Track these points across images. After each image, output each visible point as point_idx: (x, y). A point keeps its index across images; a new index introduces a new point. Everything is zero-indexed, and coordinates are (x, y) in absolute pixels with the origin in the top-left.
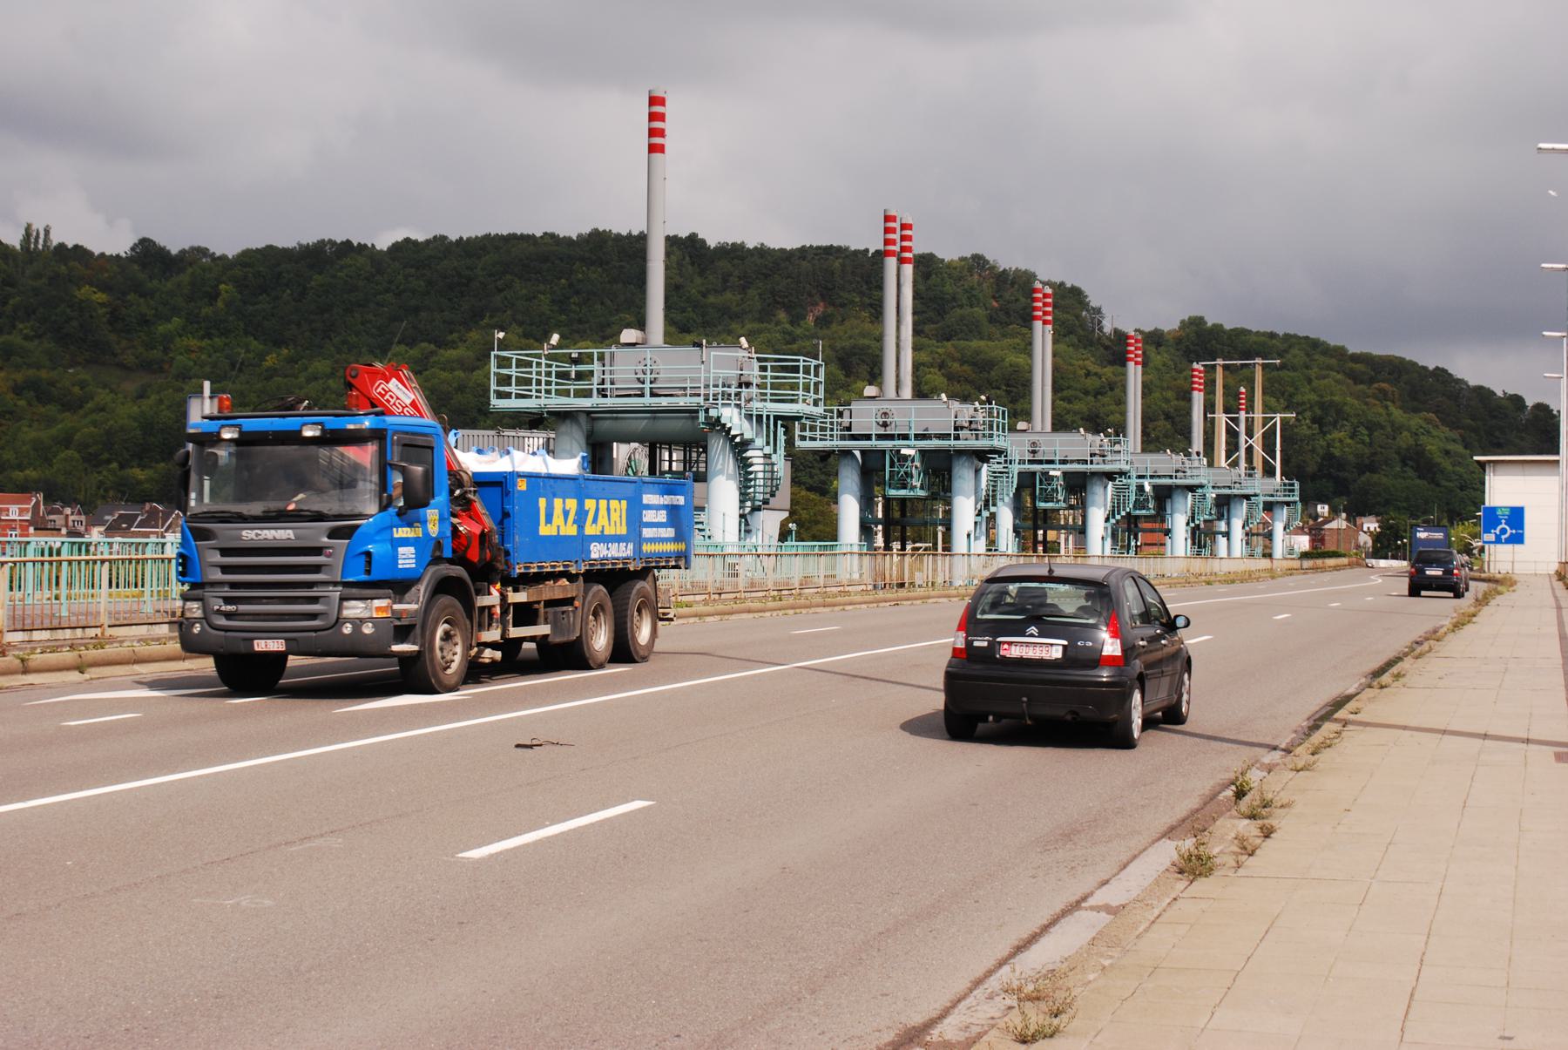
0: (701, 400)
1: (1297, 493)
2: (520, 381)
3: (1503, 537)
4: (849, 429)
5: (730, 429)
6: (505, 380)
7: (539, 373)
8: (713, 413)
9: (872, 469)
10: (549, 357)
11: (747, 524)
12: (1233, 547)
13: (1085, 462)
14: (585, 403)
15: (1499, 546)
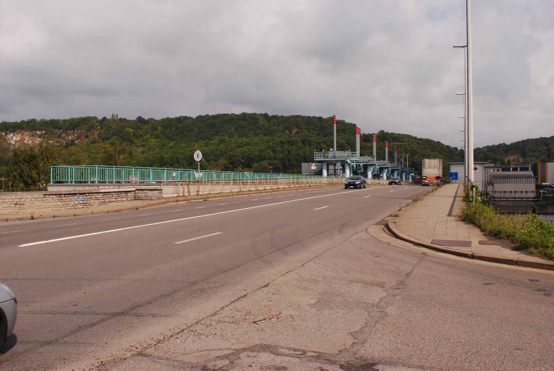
13: (367, 162)
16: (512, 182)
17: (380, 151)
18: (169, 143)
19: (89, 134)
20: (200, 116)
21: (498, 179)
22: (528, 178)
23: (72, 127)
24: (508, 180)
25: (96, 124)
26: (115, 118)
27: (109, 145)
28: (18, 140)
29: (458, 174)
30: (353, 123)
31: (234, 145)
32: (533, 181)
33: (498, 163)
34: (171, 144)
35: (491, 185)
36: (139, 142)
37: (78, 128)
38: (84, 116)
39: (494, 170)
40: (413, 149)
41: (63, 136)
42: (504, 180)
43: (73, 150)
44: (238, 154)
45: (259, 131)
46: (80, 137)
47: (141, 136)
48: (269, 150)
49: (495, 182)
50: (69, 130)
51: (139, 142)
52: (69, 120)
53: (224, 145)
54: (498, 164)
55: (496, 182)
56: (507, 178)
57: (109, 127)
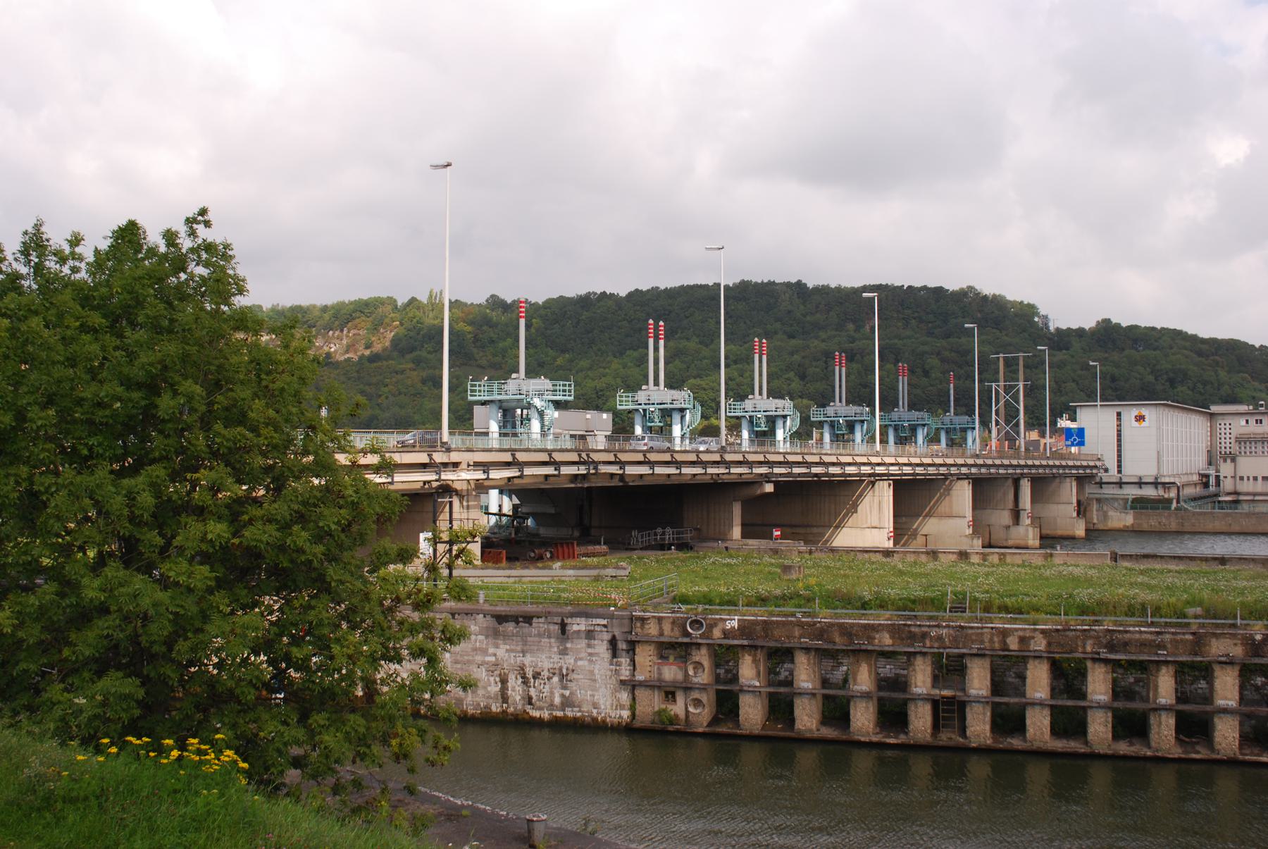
9: (948, 432)
16: (1256, 452)
17: (1084, 372)
18: (555, 359)
19: (373, 339)
20: (941, 287)
21: (1248, 443)
23: (337, 323)
25: (392, 315)
26: (436, 298)
27: (411, 365)
29: (1087, 433)
30: (1026, 303)
31: (706, 361)
33: (1263, 402)
34: (559, 361)
35: (1229, 461)
36: (486, 356)
37: (350, 324)
38: (365, 296)
39: (1247, 422)
40: (1178, 366)
41: (317, 344)
43: (325, 377)
44: (711, 384)
45: (778, 325)
46: (354, 345)
47: (492, 341)
48: (791, 374)
49: (1240, 453)
50: (331, 329)
51: (486, 356)
52: (333, 307)
53: (682, 362)
54: (1262, 406)
57: (418, 322)
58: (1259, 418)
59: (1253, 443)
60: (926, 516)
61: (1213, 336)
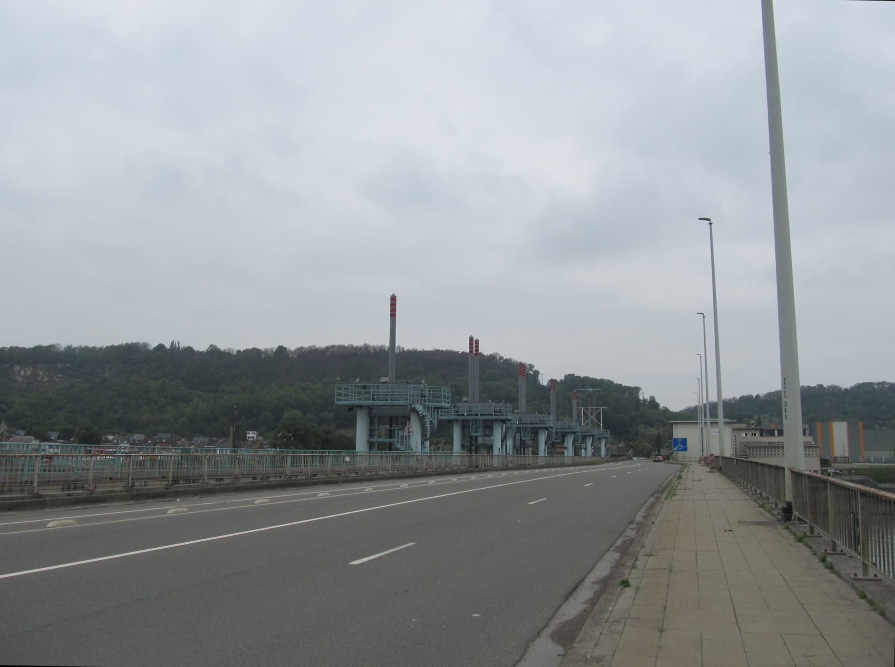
0: (408, 402)
1: (609, 434)
2: (346, 395)
3: (680, 449)
4: (457, 412)
5: (418, 412)
6: (340, 395)
7: (352, 392)
8: (412, 406)
9: (464, 425)
10: (356, 386)
11: (424, 444)
12: (588, 451)
13: (492, 415)
14: (368, 403)
15: (679, 452)
22: (811, 448)
24: (771, 451)
28: (28, 375)
32: (814, 452)
39: (746, 434)
42: (765, 451)
49: (750, 455)
54: (753, 424)
55: (752, 455)
56: (770, 448)
58: (754, 432)
59: (758, 449)
60: (672, 495)
61: (606, 377)
